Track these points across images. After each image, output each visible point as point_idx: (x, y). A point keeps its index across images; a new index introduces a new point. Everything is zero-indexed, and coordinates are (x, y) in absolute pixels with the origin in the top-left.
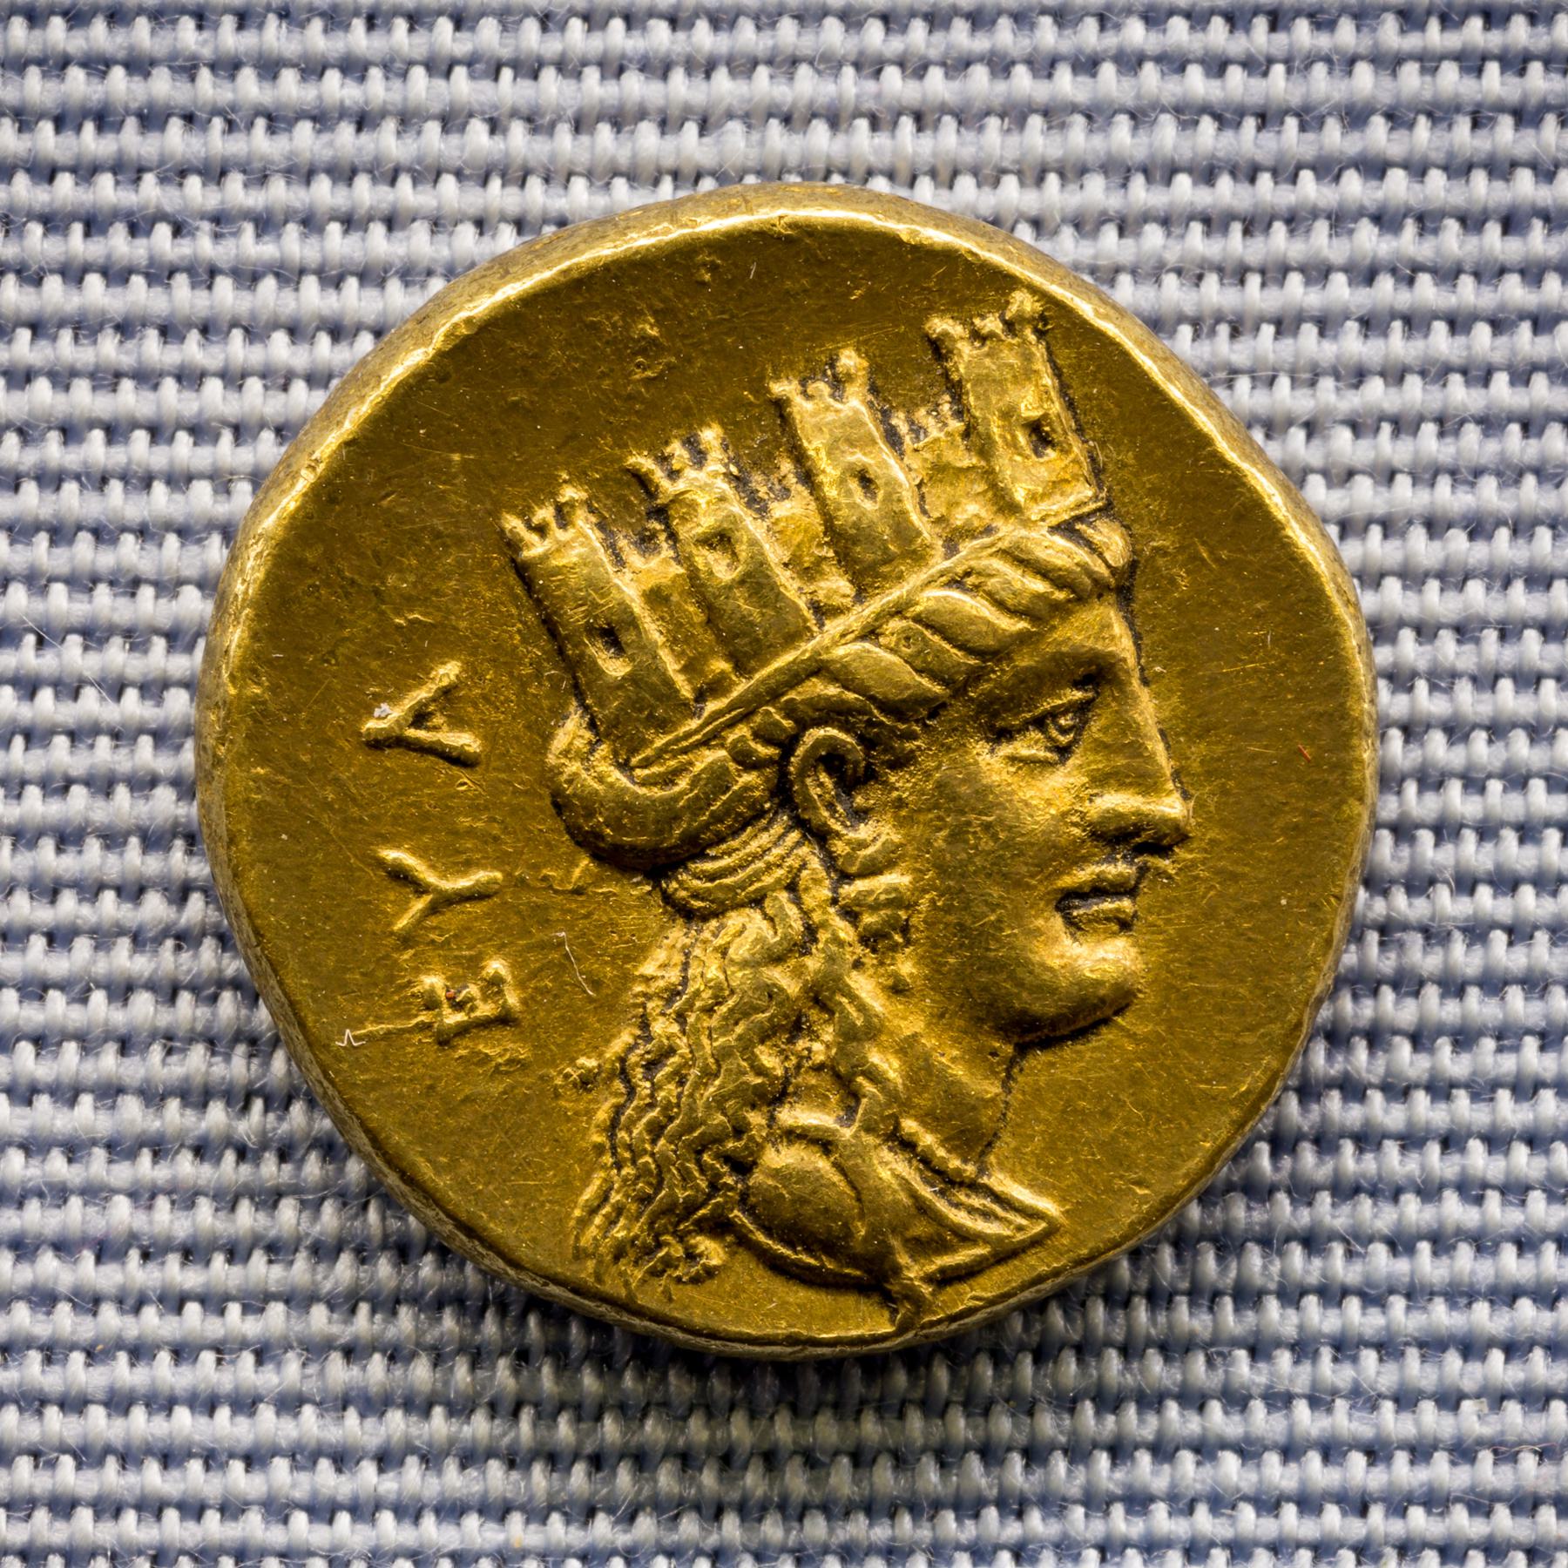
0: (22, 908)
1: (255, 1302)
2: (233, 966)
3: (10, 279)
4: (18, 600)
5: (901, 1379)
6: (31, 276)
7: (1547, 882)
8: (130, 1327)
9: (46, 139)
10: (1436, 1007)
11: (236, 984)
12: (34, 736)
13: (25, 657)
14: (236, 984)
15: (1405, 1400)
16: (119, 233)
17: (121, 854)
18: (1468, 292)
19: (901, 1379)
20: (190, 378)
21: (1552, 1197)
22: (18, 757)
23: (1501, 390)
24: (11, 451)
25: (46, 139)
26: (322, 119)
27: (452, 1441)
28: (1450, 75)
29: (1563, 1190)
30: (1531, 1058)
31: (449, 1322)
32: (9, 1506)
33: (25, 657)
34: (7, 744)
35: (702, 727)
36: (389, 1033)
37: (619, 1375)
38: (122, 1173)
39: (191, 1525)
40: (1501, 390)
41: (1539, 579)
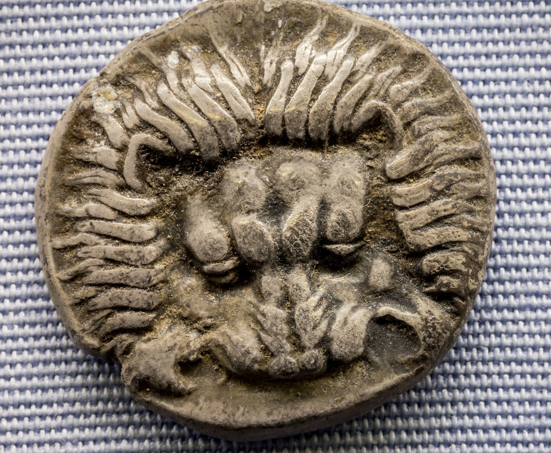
0: (5, 170)
2: (71, 343)
5: (316, 439)
7: (545, 121)
10: (509, 287)
11: (72, 347)
12: (8, 99)
13: (7, 51)
14: (72, 347)
15: (497, 429)
16: (29, 48)
18: (528, 60)
19: (316, 439)
20: (37, 430)
21: (547, 230)
28: (525, 18)
29: (548, 161)
30: (541, 194)
31: (154, 429)
33: (7, 51)
38: (37, 344)
39: (86, 33)
41: (543, 402)
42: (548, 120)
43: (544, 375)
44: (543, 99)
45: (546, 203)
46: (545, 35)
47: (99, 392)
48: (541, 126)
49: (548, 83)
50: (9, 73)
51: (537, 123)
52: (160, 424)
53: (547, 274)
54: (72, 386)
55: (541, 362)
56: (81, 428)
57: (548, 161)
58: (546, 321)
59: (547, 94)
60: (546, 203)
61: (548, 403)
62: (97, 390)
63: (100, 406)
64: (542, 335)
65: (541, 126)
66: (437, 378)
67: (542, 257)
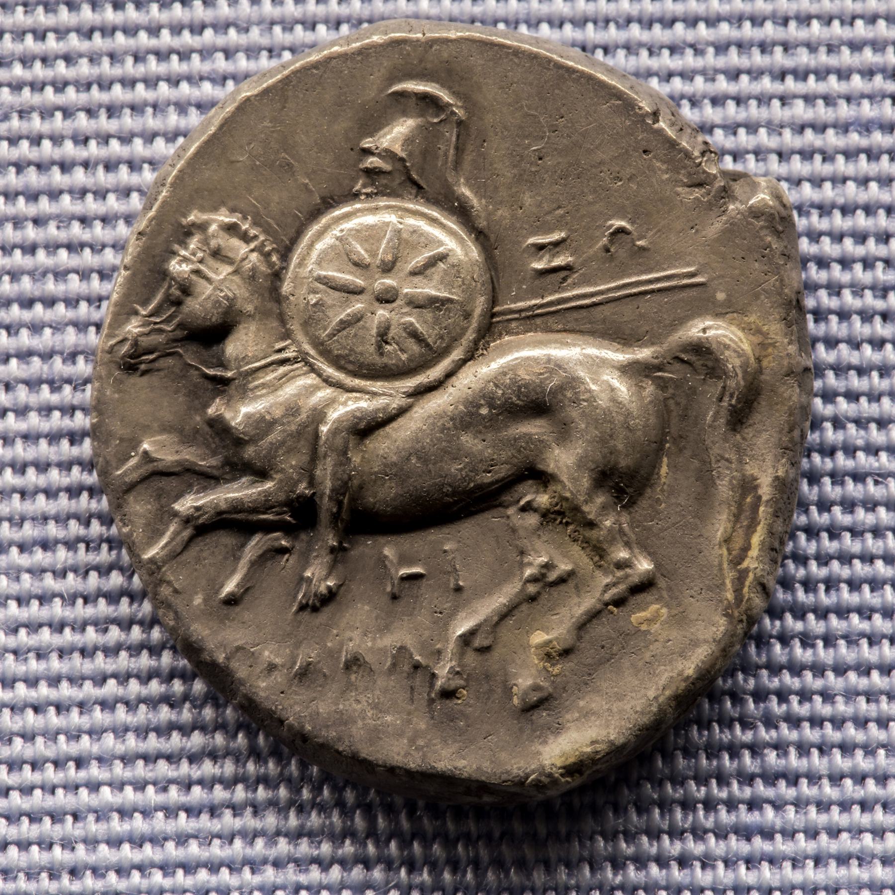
1: (101, 679)
3: (6, 525)
4: (8, 44)
6: (15, 275)
8: (50, 802)
9: (22, 394)
17: (46, 229)
22: (9, 233)
23: (857, 81)
24: (6, 531)
25: (22, 394)
26: (136, 108)
27: (182, 749)
29: (890, 559)
32: (3, 249)
34: (4, 605)
35: (311, 246)
36: (156, 199)
37: (266, 763)
40: (857, 81)
41: (878, 46)
42: (890, 421)
43: (882, 423)
44: (878, 138)
45: (886, 401)
46: (881, 251)
47: (135, 606)
48: (876, 435)
49: (888, 589)
50: (20, 166)
51: (868, 673)
52: (231, 728)
53: (888, 652)
54: (100, 594)
55: (874, 397)
56: (43, 413)
57: (890, 559)
58: (885, 316)
59: (888, 613)
60: (886, 401)
61: (892, 724)
62: (131, 603)
63: (136, 633)
64: (878, 344)
65: (876, 435)
66: (671, 811)
67: (877, 618)
